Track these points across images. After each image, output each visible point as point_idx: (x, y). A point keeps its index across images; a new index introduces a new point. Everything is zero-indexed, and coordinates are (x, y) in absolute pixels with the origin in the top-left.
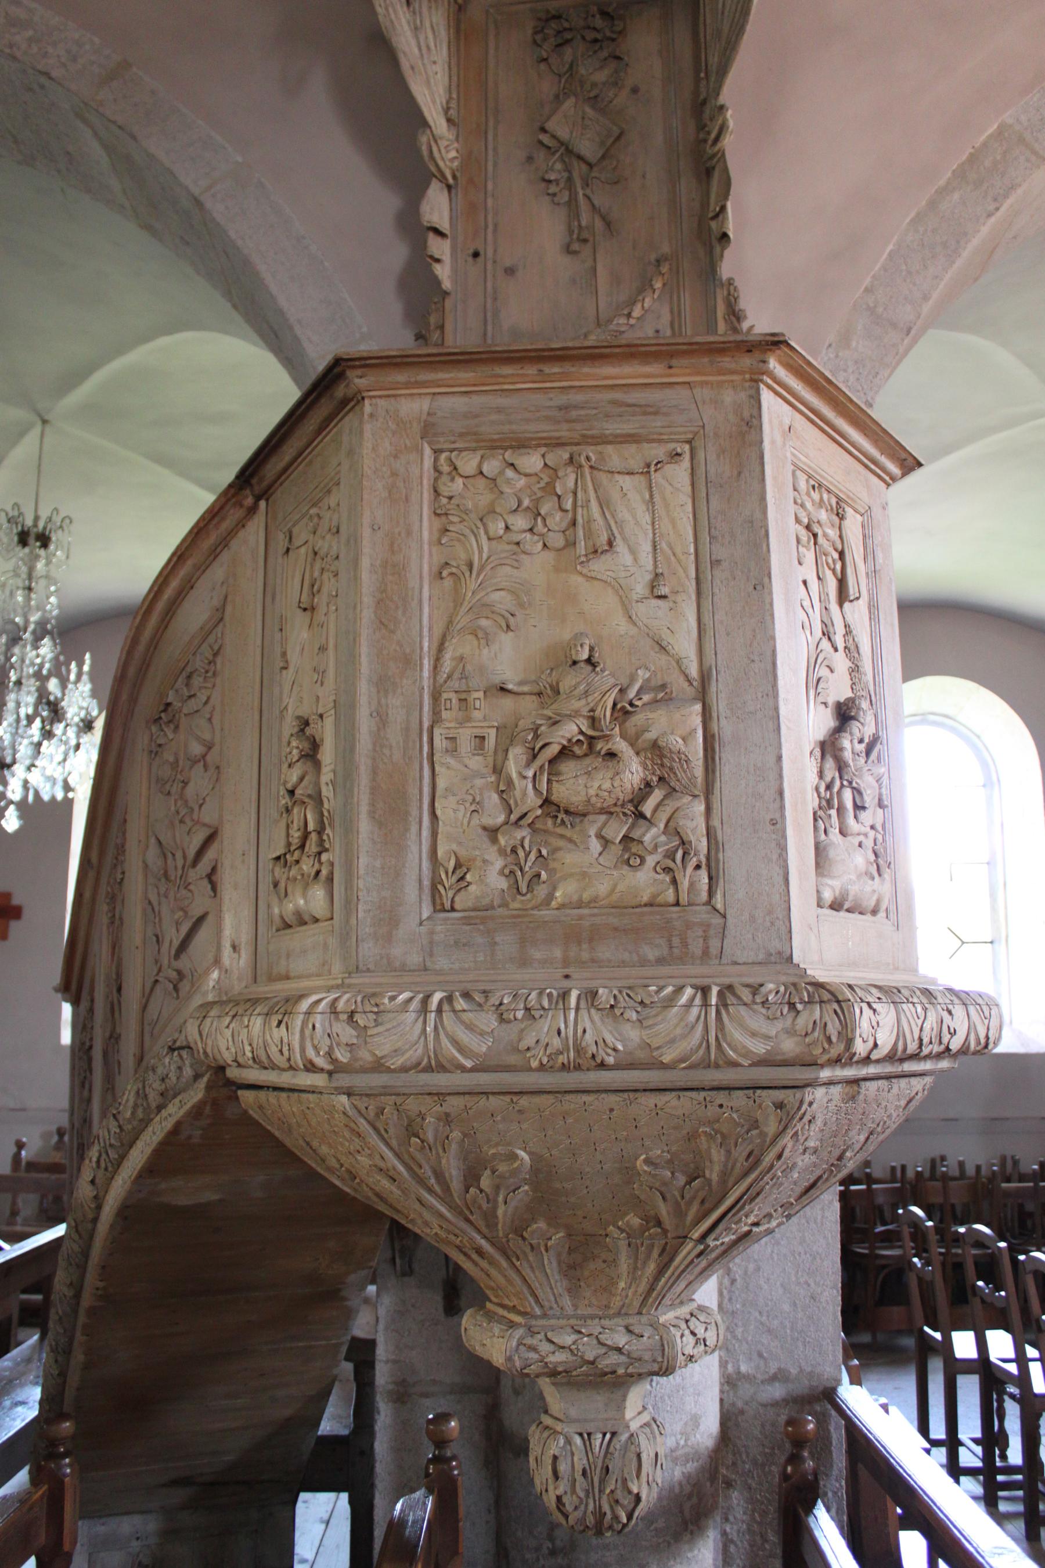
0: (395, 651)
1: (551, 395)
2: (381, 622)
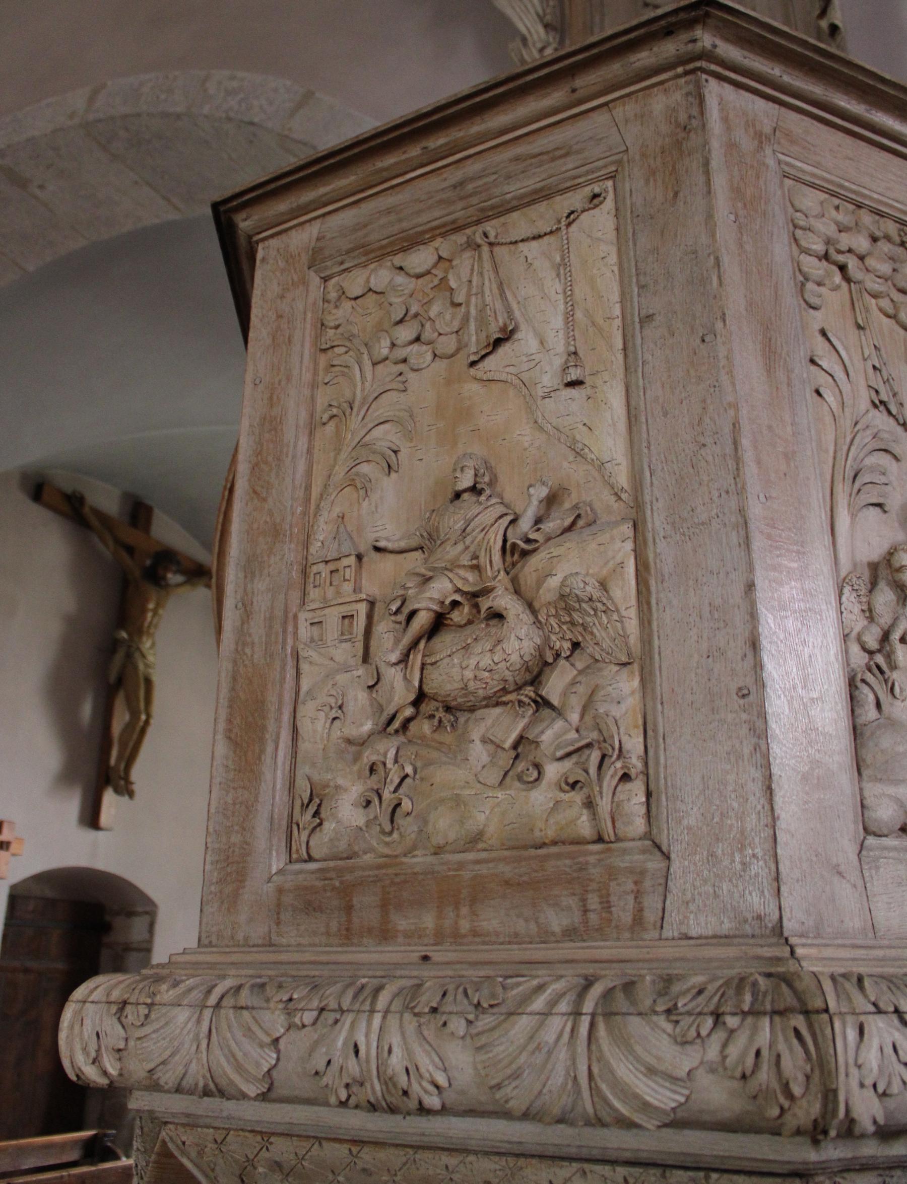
0: (266, 522)
1: (445, 176)
2: (255, 492)
